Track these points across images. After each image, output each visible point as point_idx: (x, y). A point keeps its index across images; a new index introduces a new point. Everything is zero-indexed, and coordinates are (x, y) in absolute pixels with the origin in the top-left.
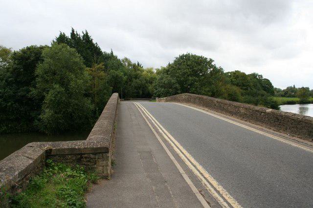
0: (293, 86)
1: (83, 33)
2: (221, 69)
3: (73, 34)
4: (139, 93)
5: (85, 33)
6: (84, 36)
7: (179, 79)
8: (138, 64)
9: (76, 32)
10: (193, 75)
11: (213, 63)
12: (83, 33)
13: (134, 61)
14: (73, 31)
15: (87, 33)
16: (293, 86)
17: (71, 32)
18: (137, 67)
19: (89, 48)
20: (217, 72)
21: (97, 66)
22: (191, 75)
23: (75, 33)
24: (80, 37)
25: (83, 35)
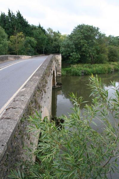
0: (7, 14)
1: (17, 12)
2: (98, 29)
3: (9, 13)
4: (56, 50)
5: (18, 12)
6: (18, 14)
7: (75, 42)
8: (58, 32)
9: (12, 12)
10: (84, 39)
11: (99, 31)
12: (17, 12)
13: (55, 30)
14: (9, 11)
15: (19, 12)
16: (7, 14)
17: (8, 11)
18: (57, 34)
19: (20, 23)
20: (102, 36)
21: (19, 34)
22: (83, 39)
23: (11, 12)
24: (14, 15)
25: (17, 13)
